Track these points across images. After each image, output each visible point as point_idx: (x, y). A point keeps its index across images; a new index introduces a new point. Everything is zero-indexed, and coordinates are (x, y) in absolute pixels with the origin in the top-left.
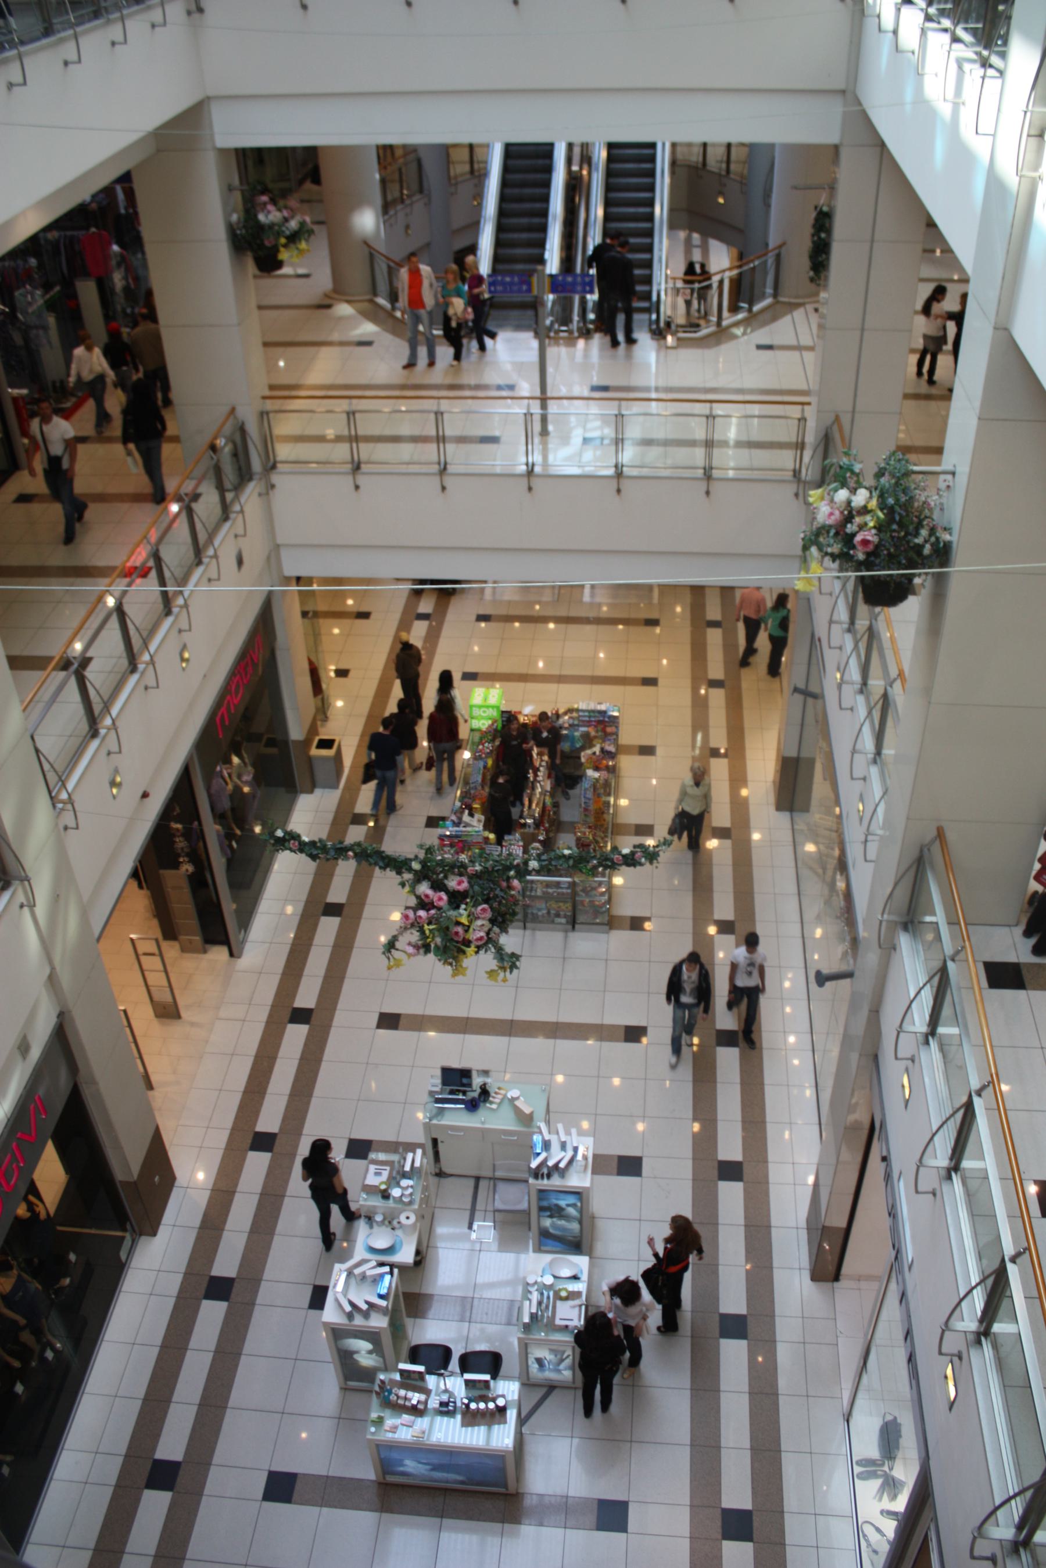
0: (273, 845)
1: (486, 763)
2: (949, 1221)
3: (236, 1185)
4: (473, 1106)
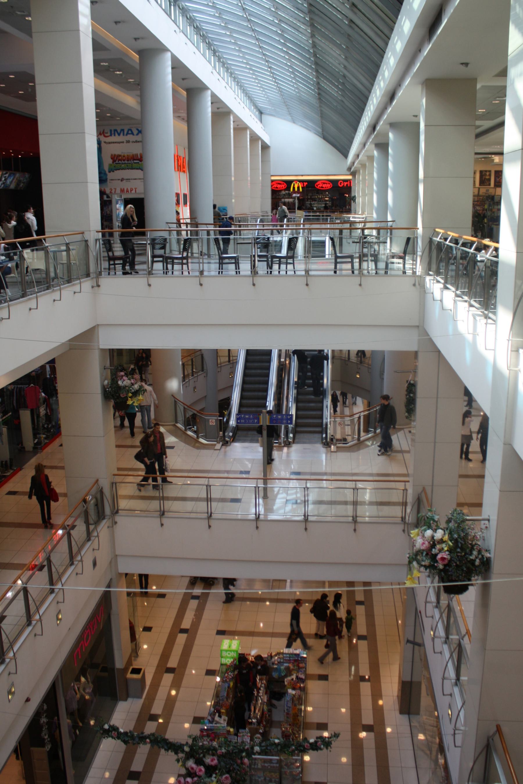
1: (229, 684)
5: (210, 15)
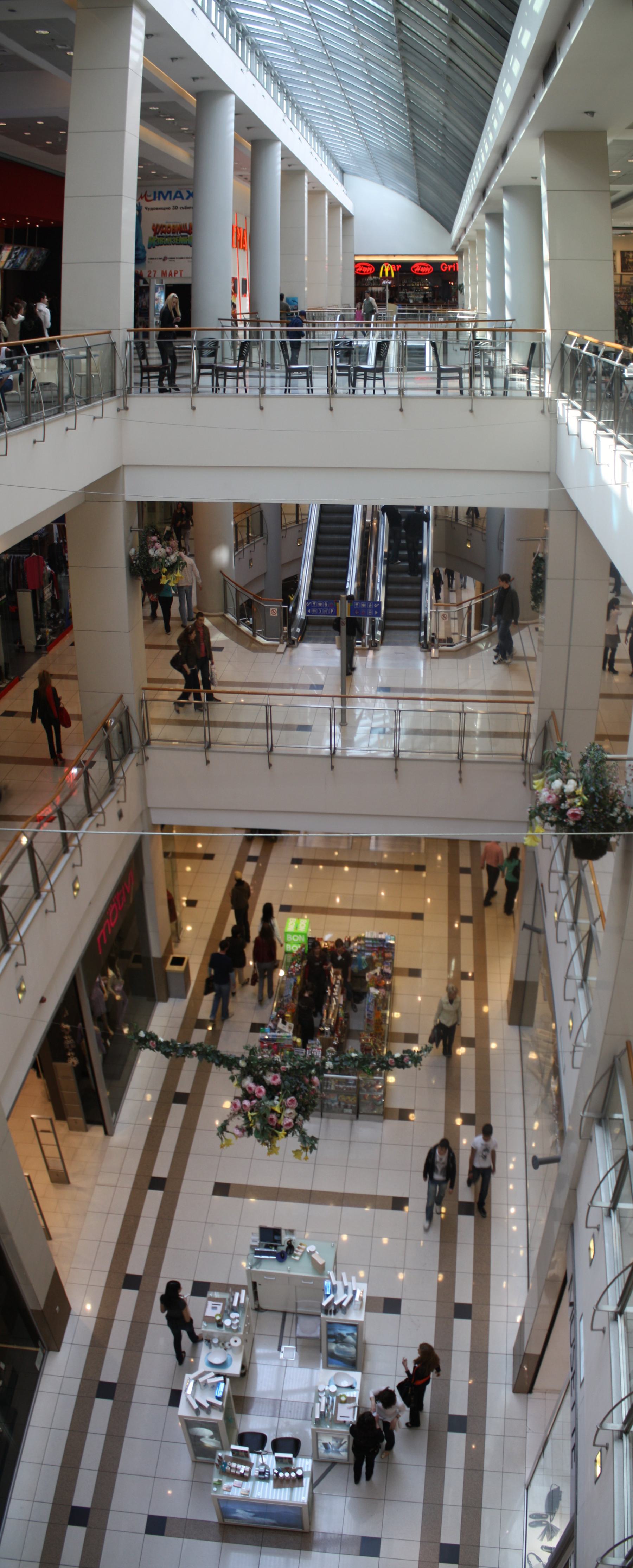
0: (137, 1044)
1: (296, 980)
2: (612, 1351)
3: (114, 1315)
4: (281, 1258)
5: (284, 52)
